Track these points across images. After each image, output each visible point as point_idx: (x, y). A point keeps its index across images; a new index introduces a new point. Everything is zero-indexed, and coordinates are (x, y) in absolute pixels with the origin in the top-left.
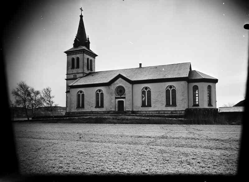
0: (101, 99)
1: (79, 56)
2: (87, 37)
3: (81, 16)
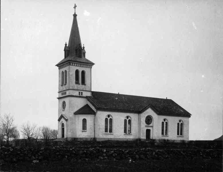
0: (108, 124)
2: (82, 47)
3: (75, 16)
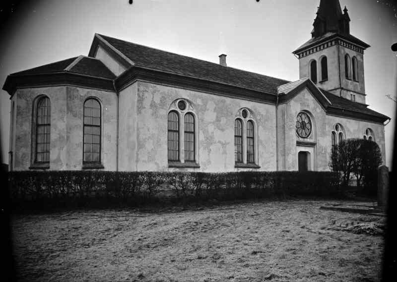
1: (324, 54)
2: (343, 9)
